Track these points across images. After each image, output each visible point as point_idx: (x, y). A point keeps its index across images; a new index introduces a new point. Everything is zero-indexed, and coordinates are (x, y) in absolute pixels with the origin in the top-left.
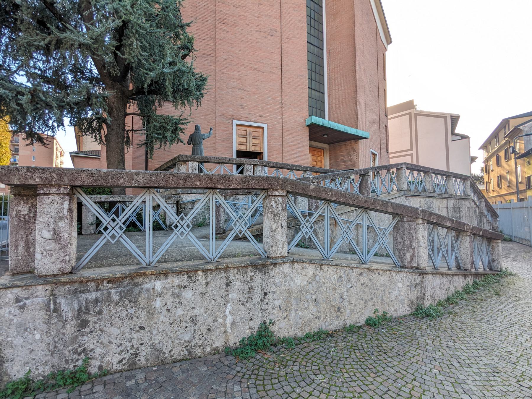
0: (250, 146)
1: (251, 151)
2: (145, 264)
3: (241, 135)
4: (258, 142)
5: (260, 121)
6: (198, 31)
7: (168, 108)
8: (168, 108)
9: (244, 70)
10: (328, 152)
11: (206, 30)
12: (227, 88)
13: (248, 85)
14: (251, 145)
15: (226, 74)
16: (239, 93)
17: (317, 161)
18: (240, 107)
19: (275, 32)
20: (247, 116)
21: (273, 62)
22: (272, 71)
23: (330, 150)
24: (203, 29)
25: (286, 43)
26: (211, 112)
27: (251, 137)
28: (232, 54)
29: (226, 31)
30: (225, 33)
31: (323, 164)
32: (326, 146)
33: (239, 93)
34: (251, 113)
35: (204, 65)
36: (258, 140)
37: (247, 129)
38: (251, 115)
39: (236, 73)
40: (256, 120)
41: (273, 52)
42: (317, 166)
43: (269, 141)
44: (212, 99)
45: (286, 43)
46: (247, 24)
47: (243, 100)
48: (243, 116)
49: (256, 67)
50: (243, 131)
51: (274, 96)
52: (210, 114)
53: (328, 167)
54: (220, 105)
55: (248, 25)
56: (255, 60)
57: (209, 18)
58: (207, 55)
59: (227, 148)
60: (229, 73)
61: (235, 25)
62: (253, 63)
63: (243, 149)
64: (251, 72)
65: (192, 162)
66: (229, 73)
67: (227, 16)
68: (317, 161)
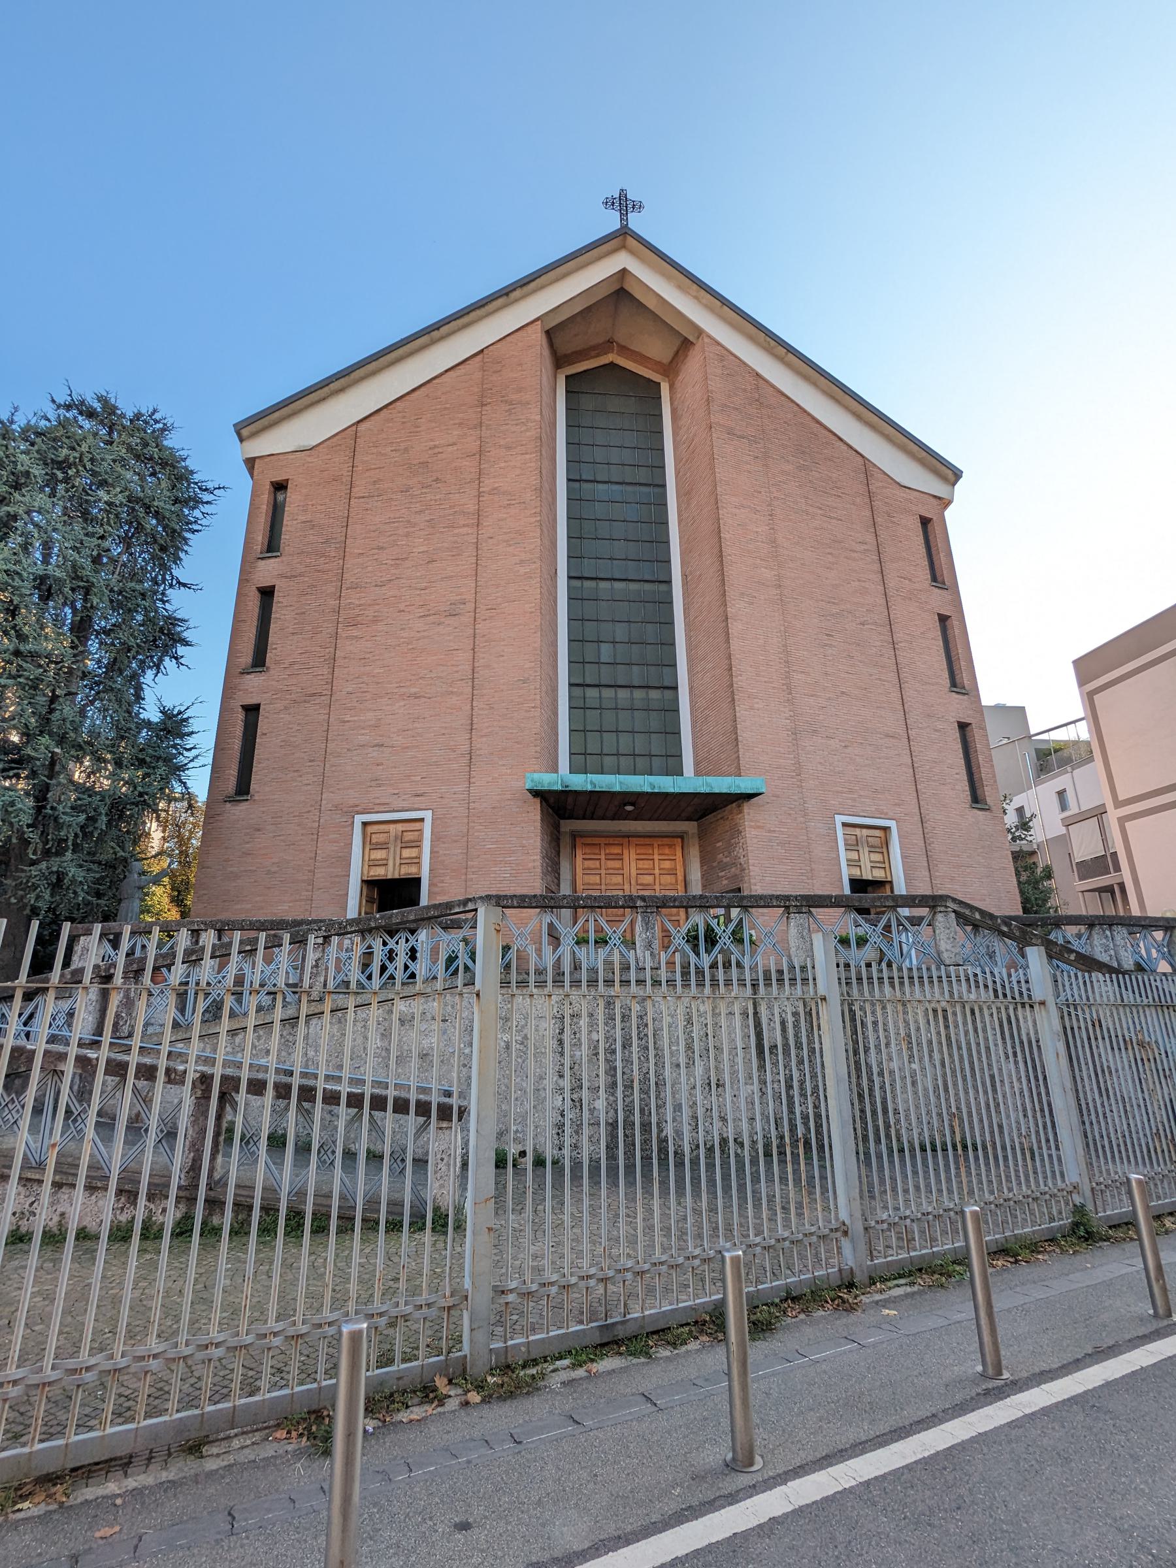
0: (394, 865)
1: (397, 876)
2: (34, 1162)
3: (377, 844)
4: (414, 855)
5: (416, 806)
6: (303, 656)
7: (234, 815)
8: (234, 815)
9: (388, 705)
10: (696, 840)
11: (318, 649)
12: (348, 750)
13: (394, 733)
14: (397, 864)
15: (348, 721)
16: (375, 754)
17: (657, 871)
18: (373, 783)
19: (462, 606)
20: (387, 801)
21: (455, 669)
22: (451, 689)
23: (702, 835)
24: (313, 649)
25: (485, 620)
26: (312, 806)
27: (399, 845)
28: (365, 679)
29: (356, 637)
30: (354, 642)
31: (680, 877)
32: (690, 827)
33: (375, 754)
34: (396, 792)
35: (307, 716)
36: (414, 849)
37: (392, 827)
38: (396, 796)
39: (370, 715)
40: (406, 805)
41: (456, 647)
42: (657, 887)
43: (436, 849)
44: (315, 779)
45: (485, 620)
46: (400, 611)
47: (381, 767)
48: (378, 801)
49: (413, 690)
50: (382, 835)
51: (452, 743)
52: (309, 812)
53: (696, 889)
54: (331, 789)
55: (403, 611)
56: (413, 677)
57: (325, 625)
58: (314, 695)
59: (337, 880)
60: (356, 718)
61: (375, 621)
62: (408, 683)
63: (379, 875)
64: (402, 703)
65: (85, 937)
66: (356, 718)
67: (361, 610)
68: (657, 871)
